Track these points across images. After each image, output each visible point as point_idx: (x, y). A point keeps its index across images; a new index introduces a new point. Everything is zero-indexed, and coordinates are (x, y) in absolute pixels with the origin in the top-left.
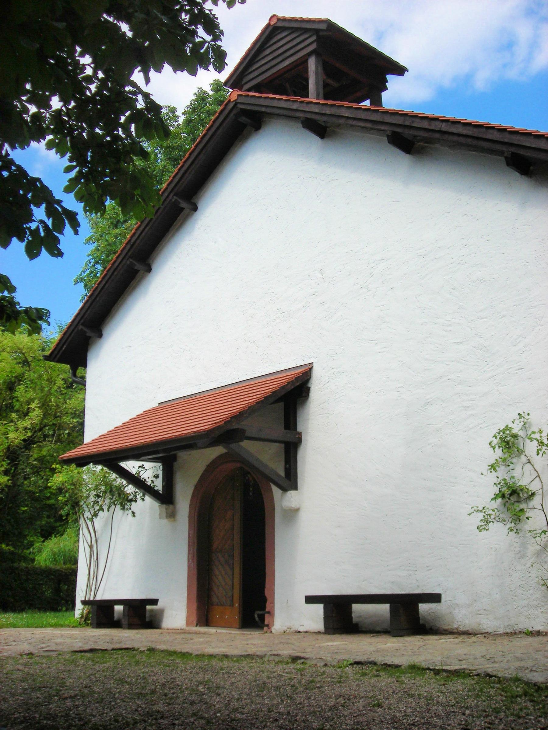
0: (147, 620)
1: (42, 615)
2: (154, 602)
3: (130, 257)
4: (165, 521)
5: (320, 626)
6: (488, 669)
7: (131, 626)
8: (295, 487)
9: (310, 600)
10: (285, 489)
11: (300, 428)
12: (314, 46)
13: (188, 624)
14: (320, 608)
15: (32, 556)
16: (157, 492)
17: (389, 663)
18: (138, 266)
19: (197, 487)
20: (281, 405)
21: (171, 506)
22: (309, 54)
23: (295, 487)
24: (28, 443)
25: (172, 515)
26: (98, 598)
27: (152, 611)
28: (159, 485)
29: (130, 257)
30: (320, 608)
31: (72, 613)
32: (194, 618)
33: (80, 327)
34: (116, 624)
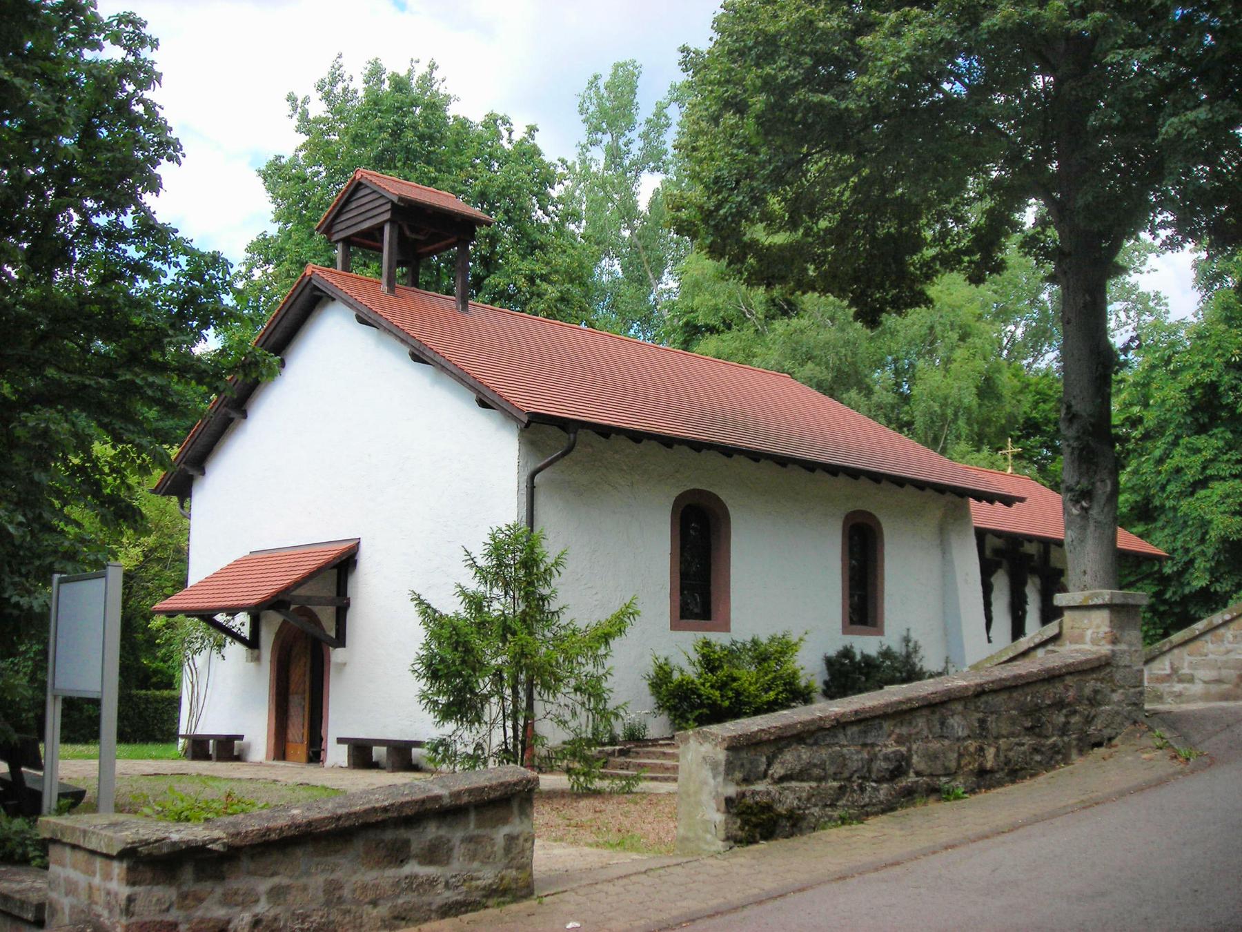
0: (235, 753)
1: (145, 746)
2: (241, 737)
3: (226, 406)
4: (252, 664)
5: (345, 764)
6: (848, 834)
7: (220, 758)
8: (344, 645)
9: (340, 741)
10: (336, 647)
11: (349, 595)
12: (387, 216)
13: (267, 757)
14: (345, 748)
15: (171, 671)
16: (245, 638)
17: (986, 840)
18: (233, 415)
19: (278, 635)
20: (335, 571)
21: (256, 651)
22: (386, 222)
23: (344, 645)
24: (141, 566)
25: (257, 659)
26: (196, 733)
27: (240, 745)
28: (246, 632)
29: (226, 406)
30: (345, 748)
31: (175, 746)
32: (272, 754)
33: (182, 466)
34: (207, 757)
